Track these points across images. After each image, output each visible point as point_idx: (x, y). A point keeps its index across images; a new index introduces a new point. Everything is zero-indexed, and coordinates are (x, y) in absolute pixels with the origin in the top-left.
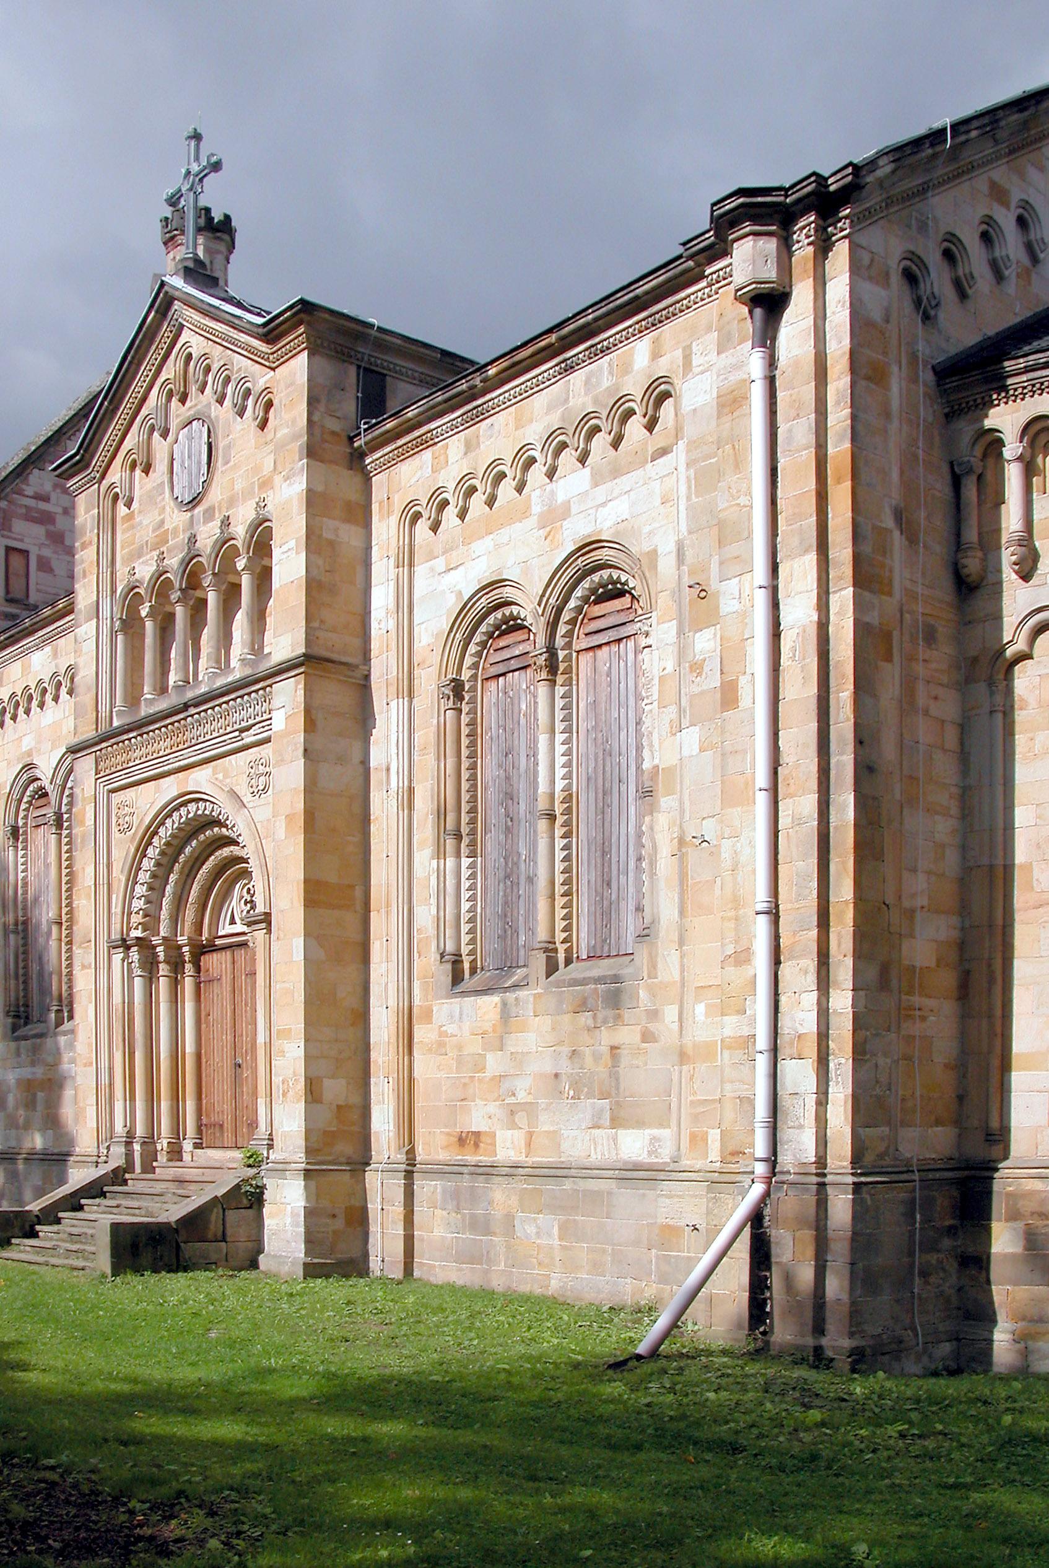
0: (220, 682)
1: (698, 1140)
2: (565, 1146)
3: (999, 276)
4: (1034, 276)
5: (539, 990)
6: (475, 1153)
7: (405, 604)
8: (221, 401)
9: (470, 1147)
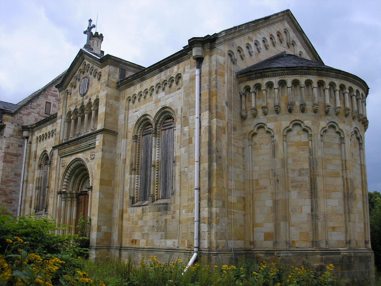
0: (86, 134)
1: (183, 242)
2: (155, 243)
3: (251, 55)
4: (259, 55)
5: (150, 206)
6: (135, 245)
7: (126, 119)
8: (91, 74)
9: (134, 244)
